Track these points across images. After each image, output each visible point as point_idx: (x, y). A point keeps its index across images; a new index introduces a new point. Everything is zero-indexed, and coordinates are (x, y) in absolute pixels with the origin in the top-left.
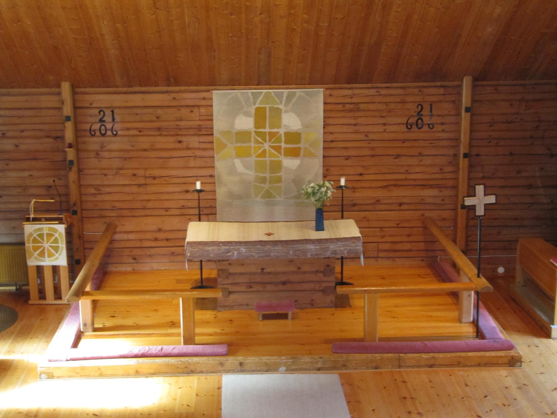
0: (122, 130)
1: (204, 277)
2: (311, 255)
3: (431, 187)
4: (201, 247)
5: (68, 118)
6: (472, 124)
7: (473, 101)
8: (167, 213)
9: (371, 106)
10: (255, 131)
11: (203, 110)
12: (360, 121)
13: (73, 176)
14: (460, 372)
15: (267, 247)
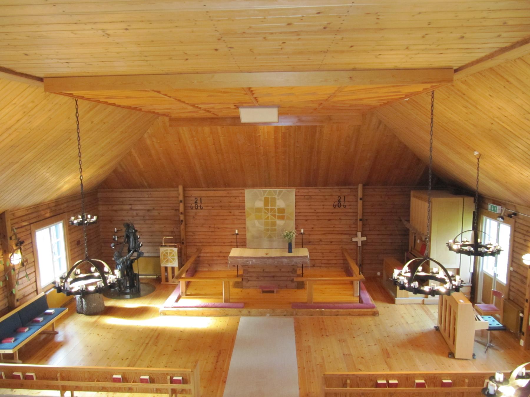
0: (205, 207)
1: (239, 274)
2: (285, 264)
3: (345, 234)
4: (235, 259)
5: (181, 201)
6: (363, 205)
7: (364, 195)
8: (224, 244)
9: (317, 197)
10: (264, 208)
11: (240, 198)
12: (312, 203)
13: (182, 227)
14: (349, 318)
15: (265, 260)
